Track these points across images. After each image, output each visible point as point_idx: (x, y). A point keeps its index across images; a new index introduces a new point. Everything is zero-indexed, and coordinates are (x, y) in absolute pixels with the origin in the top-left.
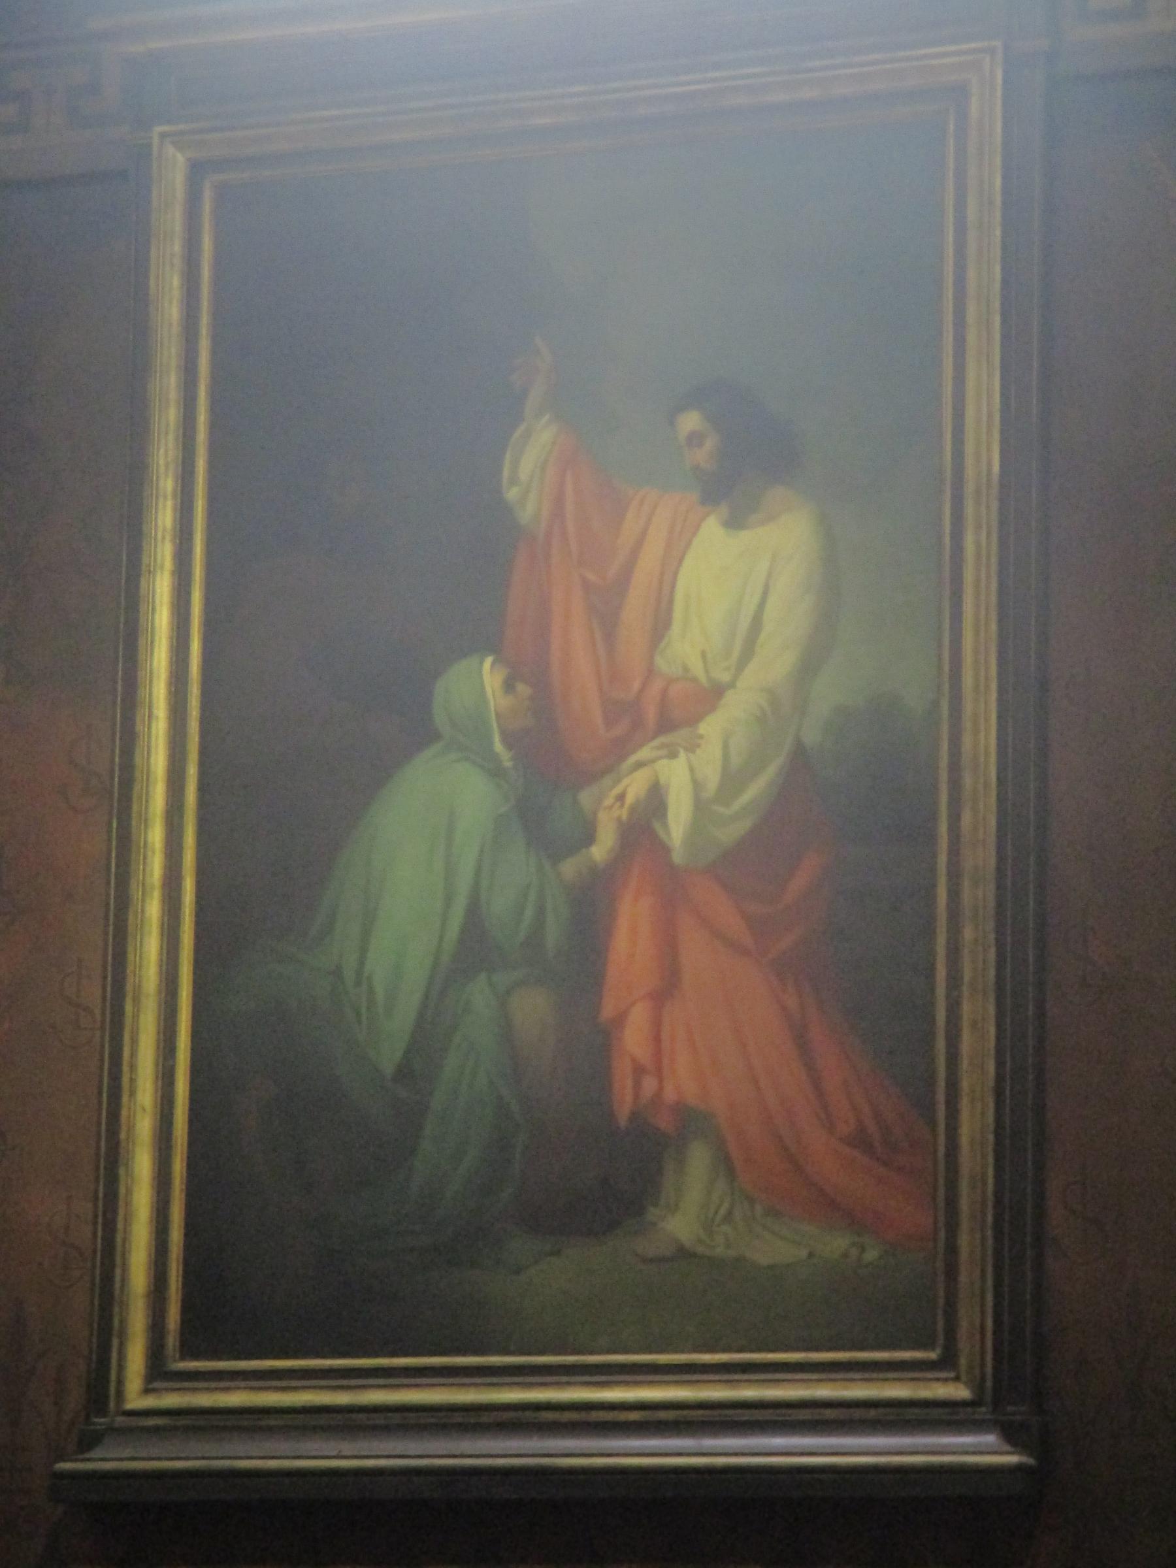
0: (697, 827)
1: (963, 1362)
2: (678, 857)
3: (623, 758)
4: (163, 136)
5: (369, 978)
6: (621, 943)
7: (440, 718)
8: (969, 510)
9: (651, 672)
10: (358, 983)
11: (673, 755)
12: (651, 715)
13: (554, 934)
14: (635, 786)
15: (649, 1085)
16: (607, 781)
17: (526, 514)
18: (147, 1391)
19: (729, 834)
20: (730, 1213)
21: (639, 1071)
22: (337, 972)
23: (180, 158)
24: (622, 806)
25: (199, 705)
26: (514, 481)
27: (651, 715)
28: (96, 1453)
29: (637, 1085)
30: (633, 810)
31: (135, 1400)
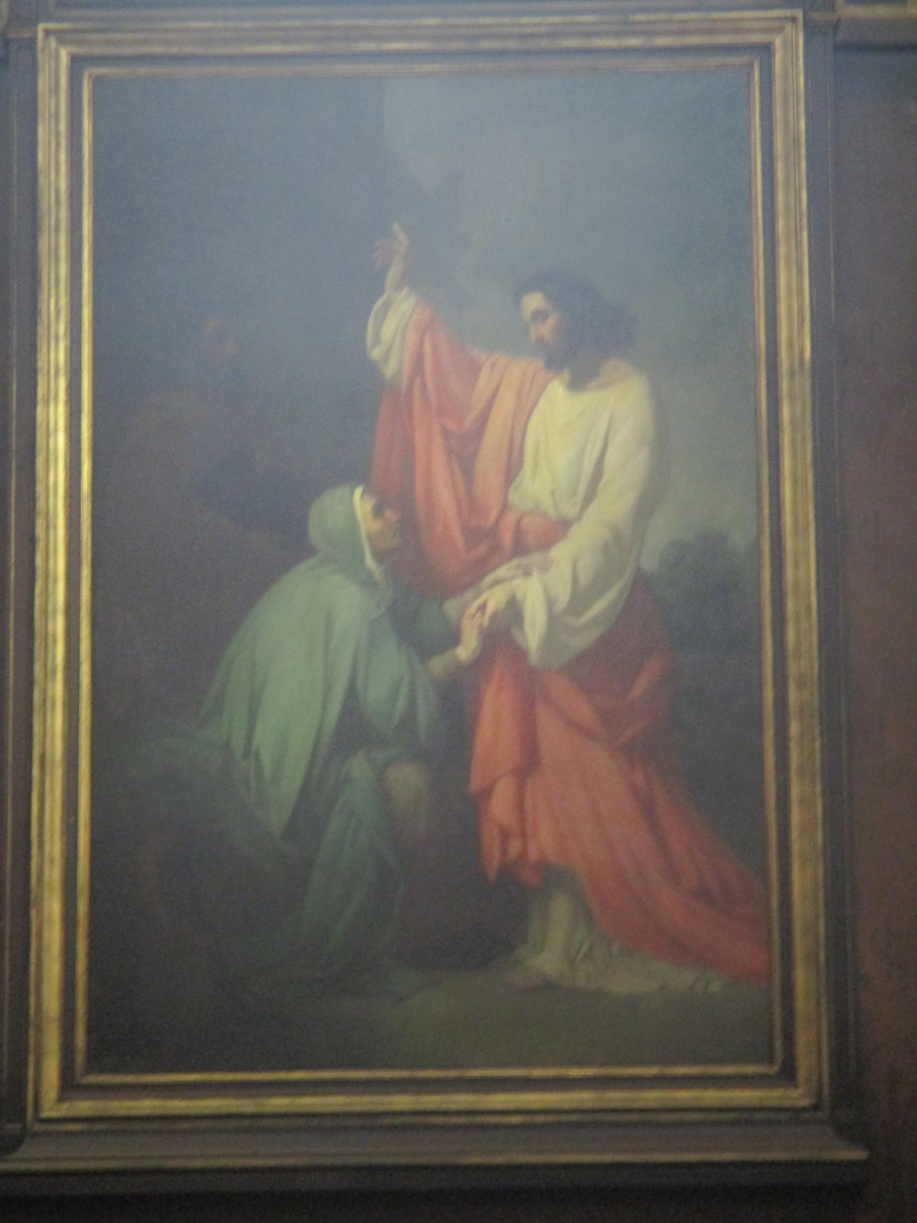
0: (549, 641)
1: (802, 1074)
2: (534, 658)
3: (483, 575)
4: (47, 33)
5: (257, 754)
6: (485, 731)
7: (315, 534)
8: (785, 385)
9: (505, 506)
10: (247, 754)
11: (527, 574)
12: (507, 538)
13: (424, 716)
14: (495, 599)
15: (515, 846)
16: (470, 594)
17: (389, 370)
18: (61, 1100)
19: (580, 642)
20: (591, 948)
21: (505, 836)
22: (227, 746)
23: (64, 54)
24: (483, 614)
25: (61, 735)
26: (377, 341)
27: (507, 538)
28: (18, 1154)
29: (504, 851)
30: (494, 617)
31: (51, 1107)
